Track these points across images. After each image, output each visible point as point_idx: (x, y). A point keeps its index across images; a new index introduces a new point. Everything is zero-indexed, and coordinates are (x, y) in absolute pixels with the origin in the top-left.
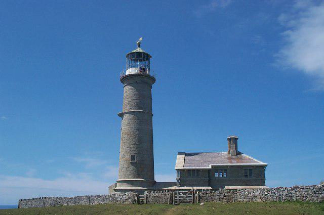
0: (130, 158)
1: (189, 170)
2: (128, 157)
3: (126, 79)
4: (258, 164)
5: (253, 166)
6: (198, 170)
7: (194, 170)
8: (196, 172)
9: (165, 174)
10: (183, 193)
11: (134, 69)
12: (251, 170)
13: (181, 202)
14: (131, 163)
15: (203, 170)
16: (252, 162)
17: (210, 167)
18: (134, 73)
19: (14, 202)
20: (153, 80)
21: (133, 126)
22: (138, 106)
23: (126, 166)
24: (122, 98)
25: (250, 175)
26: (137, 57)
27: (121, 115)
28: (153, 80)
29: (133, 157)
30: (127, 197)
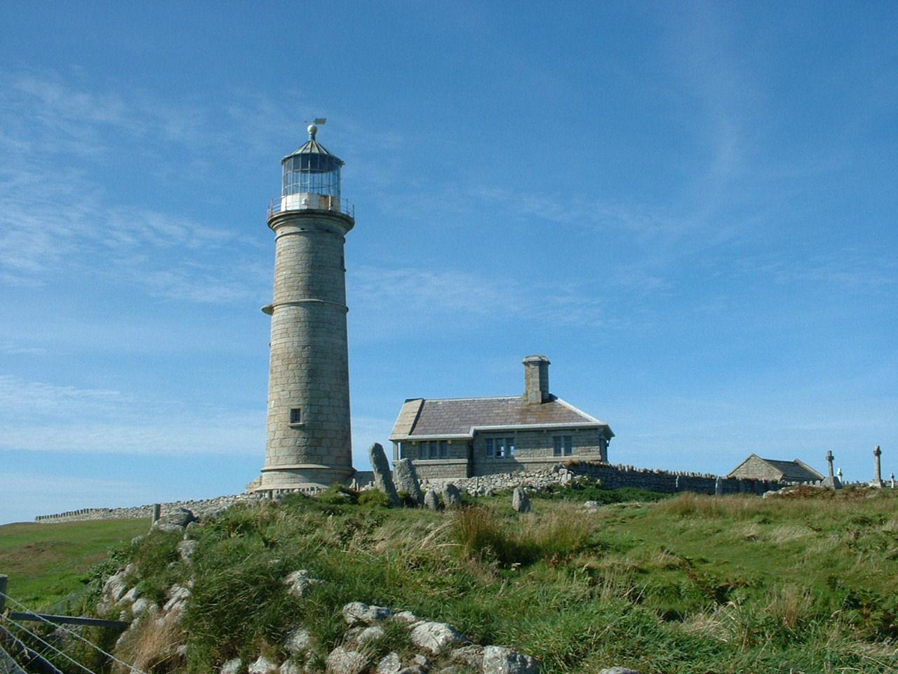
0: (288, 417)
1: (422, 442)
2: (285, 414)
3: (290, 217)
4: (586, 424)
5: (573, 429)
6: (444, 441)
7: (433, 442)
8: (438, 447)
9: (375, 427)
10: (456, 467)
11: (297, 196)
12: (568, 438)
13: (442, 447)
14: (292, 427)
15: (454, 441)
16: (572, 419)
18: (298, 208)
19: (31, 519)
20: (348, 222)
21: (296, 339)
22: (309, 455)
23: (279, 434)
24: (274, 255)
26: (304, 165)
27: (269, 310)
28: (348, 222)
29: (295, 414)
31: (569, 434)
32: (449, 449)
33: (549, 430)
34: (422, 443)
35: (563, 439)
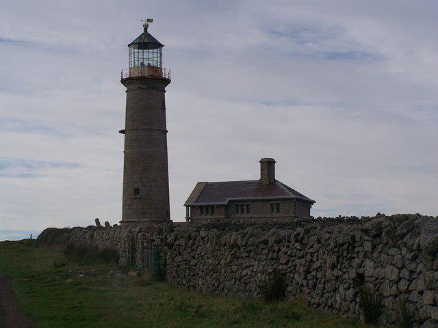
7: (207, 207)
17: (226, 203)
25: (278, 211)
31: (278, 202)
33: (268, 200)
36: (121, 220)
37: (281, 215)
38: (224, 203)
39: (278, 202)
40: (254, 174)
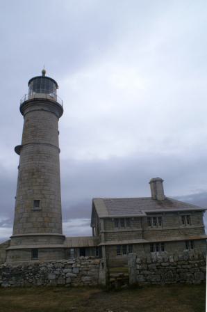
12: (160, 218)
30: (76, 271)
32: (131, 222)
34: (116, 219)
35: (186, 217)
36: (11, 235)
37: (193, 226)
38: (141, 215)
39: (161, 215)
40: (147, 193)
